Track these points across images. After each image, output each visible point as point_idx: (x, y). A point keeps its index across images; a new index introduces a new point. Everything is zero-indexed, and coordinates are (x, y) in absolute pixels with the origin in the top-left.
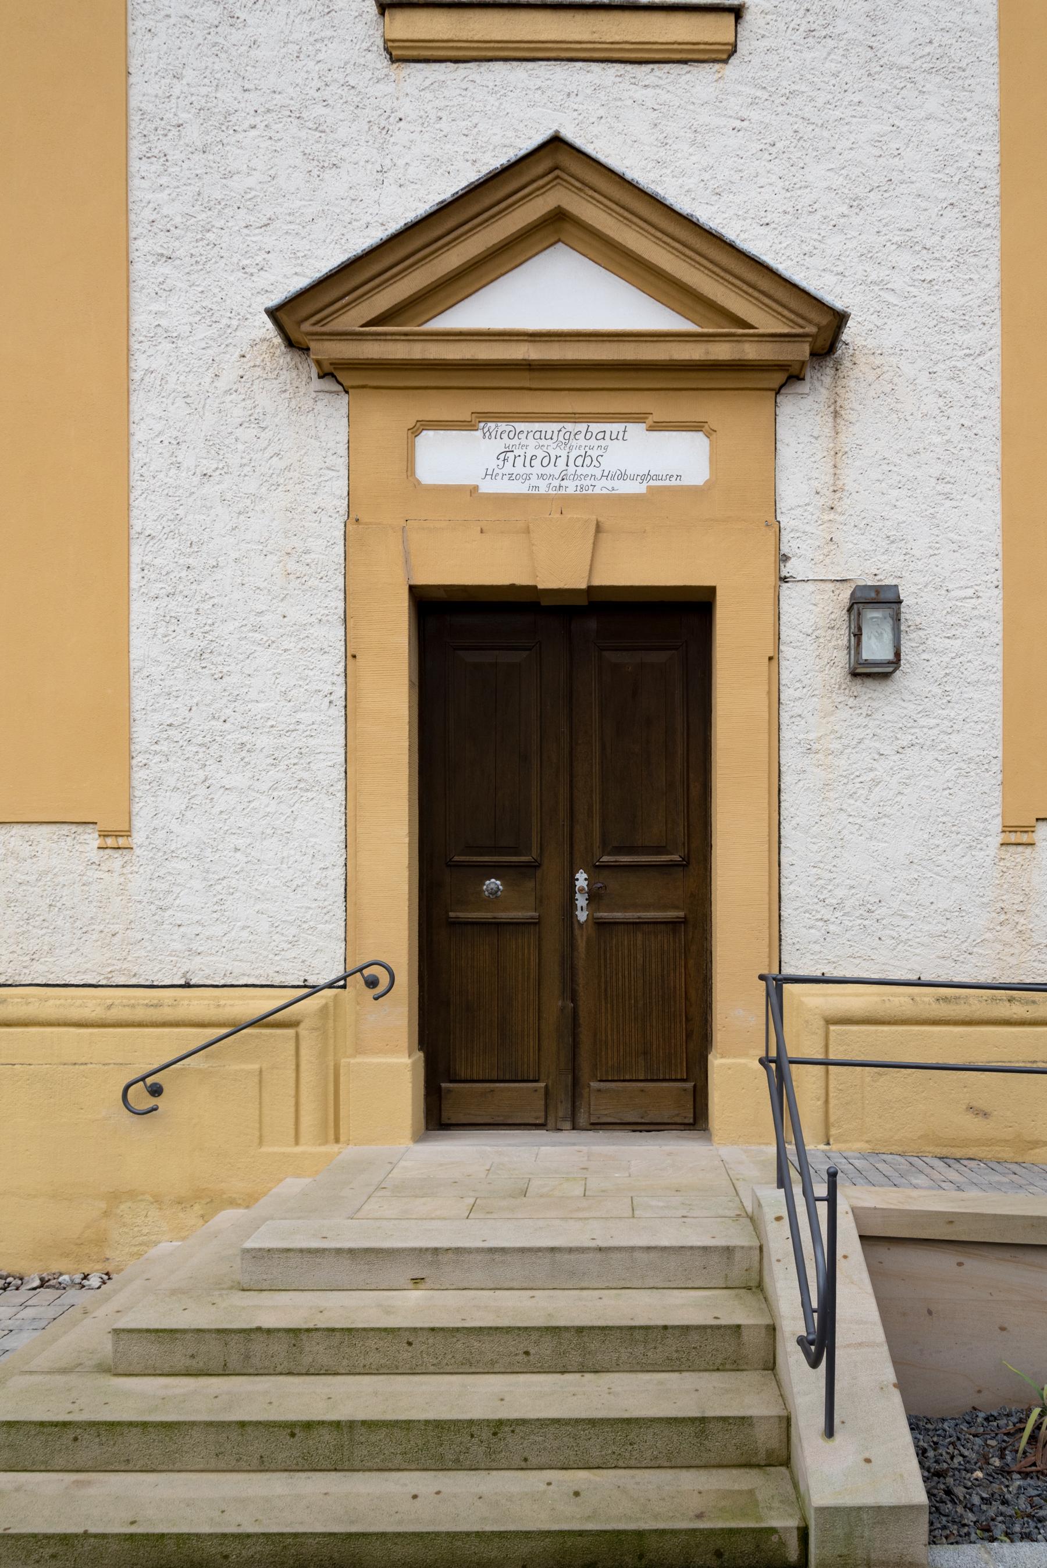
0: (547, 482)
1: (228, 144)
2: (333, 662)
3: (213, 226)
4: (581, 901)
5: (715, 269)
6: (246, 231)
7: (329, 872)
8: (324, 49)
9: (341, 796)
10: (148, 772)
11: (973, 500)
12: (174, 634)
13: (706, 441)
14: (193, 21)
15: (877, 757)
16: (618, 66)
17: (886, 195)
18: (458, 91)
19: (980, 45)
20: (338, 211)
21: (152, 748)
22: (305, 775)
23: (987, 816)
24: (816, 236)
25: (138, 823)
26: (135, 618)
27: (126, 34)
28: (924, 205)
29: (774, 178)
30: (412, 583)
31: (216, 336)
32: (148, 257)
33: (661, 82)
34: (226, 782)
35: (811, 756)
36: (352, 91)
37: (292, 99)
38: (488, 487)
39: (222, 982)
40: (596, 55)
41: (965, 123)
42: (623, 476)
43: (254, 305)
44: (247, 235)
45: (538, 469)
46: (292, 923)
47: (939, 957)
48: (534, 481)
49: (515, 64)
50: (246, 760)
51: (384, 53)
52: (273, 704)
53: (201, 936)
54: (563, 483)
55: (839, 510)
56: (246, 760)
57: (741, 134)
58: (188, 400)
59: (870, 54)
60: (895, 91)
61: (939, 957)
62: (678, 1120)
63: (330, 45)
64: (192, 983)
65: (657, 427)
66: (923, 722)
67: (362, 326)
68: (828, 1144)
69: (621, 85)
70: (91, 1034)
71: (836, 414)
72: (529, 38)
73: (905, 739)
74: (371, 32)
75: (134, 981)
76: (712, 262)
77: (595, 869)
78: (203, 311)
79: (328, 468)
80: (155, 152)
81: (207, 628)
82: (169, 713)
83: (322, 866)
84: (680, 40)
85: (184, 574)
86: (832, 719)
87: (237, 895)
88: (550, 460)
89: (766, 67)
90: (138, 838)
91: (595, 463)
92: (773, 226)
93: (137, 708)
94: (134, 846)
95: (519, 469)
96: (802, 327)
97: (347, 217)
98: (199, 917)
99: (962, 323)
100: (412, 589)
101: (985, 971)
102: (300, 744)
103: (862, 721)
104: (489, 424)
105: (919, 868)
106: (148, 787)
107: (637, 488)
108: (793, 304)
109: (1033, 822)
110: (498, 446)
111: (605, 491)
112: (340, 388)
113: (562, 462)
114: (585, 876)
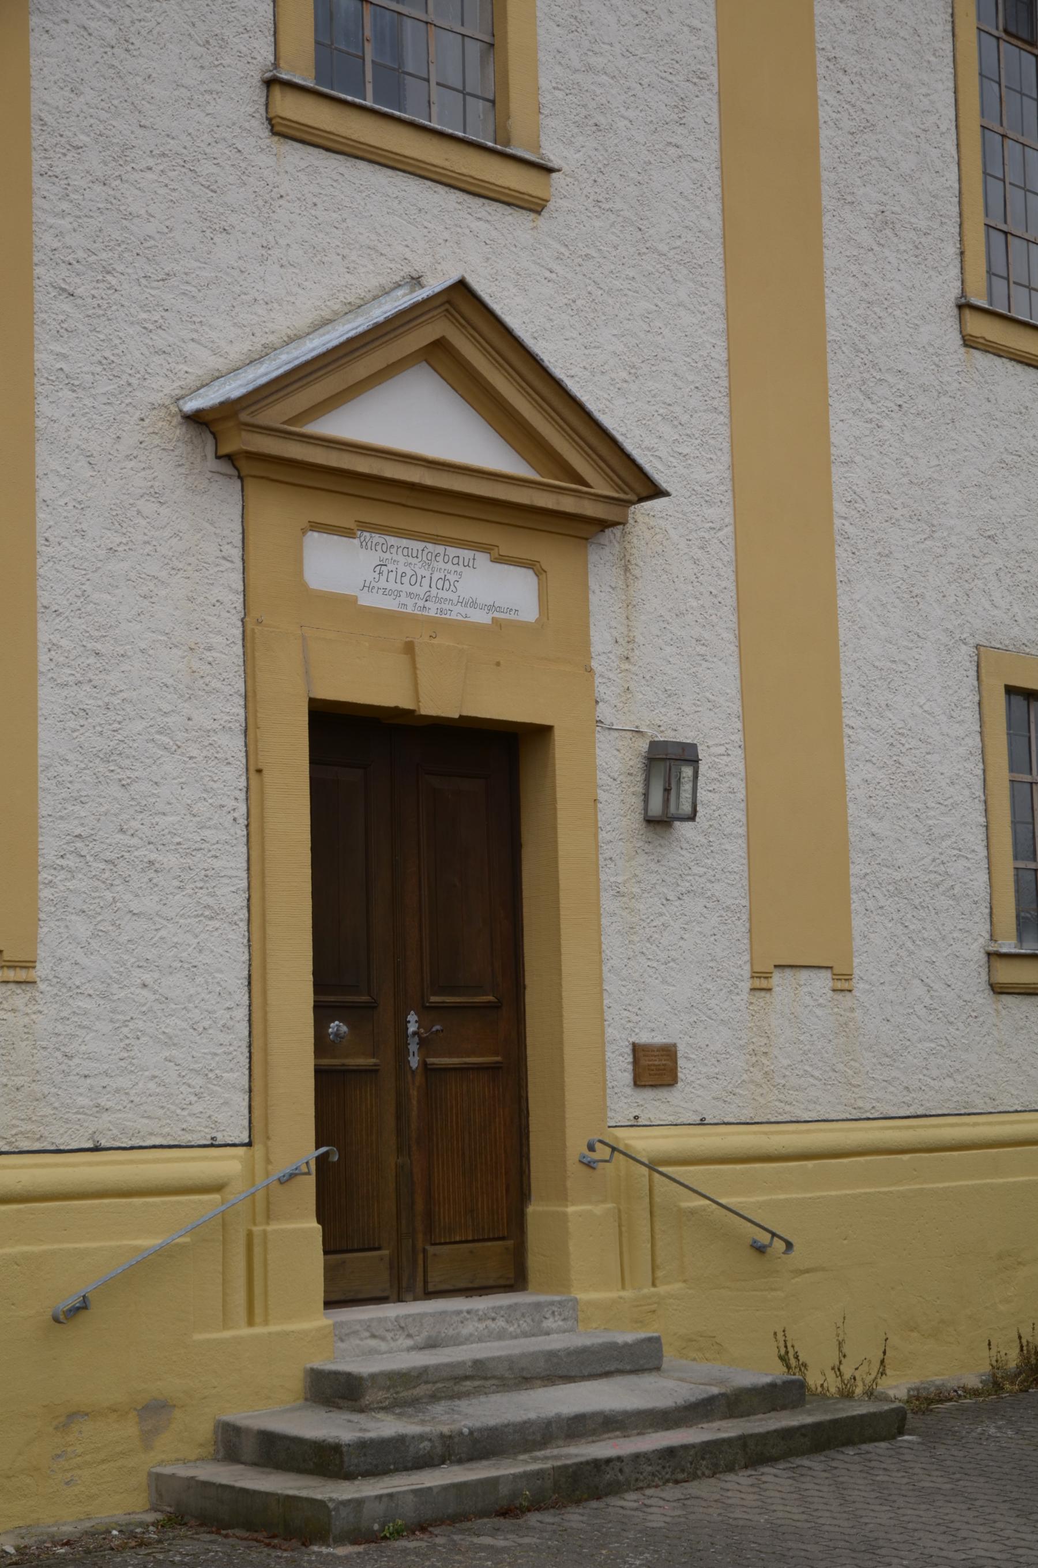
0: (414, 601)
1: (127, 181)
2: (234, 776)
3: (114, 269)
4: (413, 1047)
5: (565, 427)
6: (143, 281)
7: (234, 1013)
8: (213, 103)
9: (243, 926)
10: (53, 890)
11: (720, 663)
12: (82, 730)
13: (535, 579)
14: (90, 34)
15: (665, 902)
16: (459, 194)
17: (654, 369)
18: (330, 182)
19: (712, 248)
20: (229, 280)
21: (58, 862)
22: (211, 901)
23: (740, 962)
24: (606, 396)
25: (42, 952)
26: (44, 707)
27: (733, 491)
28: (679, 383)
29: (575, 334)
30: (312, 696)
31: (117, 392)
32: (50, 289)
33: (489, 218)
34: (135, 906)
35: (620, 899)
36: (238, 154)
37: (185, 148)
38: (366, 600)
39: (130, 1144)
40: (444, 180)
41: (704, 316)
42: (474, 604)
43: (152, 365)
44: (146, 287)
45: (407, 588)
46: (197, 1072)
47: (714, 1098)
48: (404, 599)
49: (377, 167)
50: (155, 881)
51: (266, 123)
52: (179, 818)
53: (108, 1089)
54: (427, 604)
55: (632, 660)
56: (155, 881)
57: (550, 284)
58: (91, 459)
59: (639, 235)
60: (657, 274)
61: (714, 1098)
62: (502, 1282)
63: (218, 100)
64: (104, 1143)
65: (500, 559)
66: (696, 870)
67: (284, 423)
68: (654, 1285)
69: (461, 213)
70: (19, 1211)
71: (626, 570)
72: (395, 150)
73: (685, 886)
74: (256, 98)
75: (37, 1146)
76: (562, 419)
77: (425, 1010)
78: (104, 361)
79: (224, 558)
80: (58, 171)
81: (116, 726)
82: (76, 822)
83: (227, 1005)
84: (512, 187)
85: (92, 660)
86: (633, 863)
87: (144, 1039)
88: (416, 580)
89: (568, 227)
90: (42, 970)
91: (452, 587)
92: (577, 379)
93: (44, 813)
94: (38, 980)
95: (391, 585)
96: (625, 493)
97: (237, 289)
98: (106, 1066)
99: (707, 498)
100: (312, 701)
101: (745, 1111)
102: (206, 866)
103: (653, 866)
104: (365, 534)
105: (697, 1011)
106: (53, 909)
107: (481, 617)
108: (624, 473)
109: (771, 968)
110: (373, 558)
111: (460, 618)
112: (236, 473)
113: (426, 582)
114: (416, 1018)
